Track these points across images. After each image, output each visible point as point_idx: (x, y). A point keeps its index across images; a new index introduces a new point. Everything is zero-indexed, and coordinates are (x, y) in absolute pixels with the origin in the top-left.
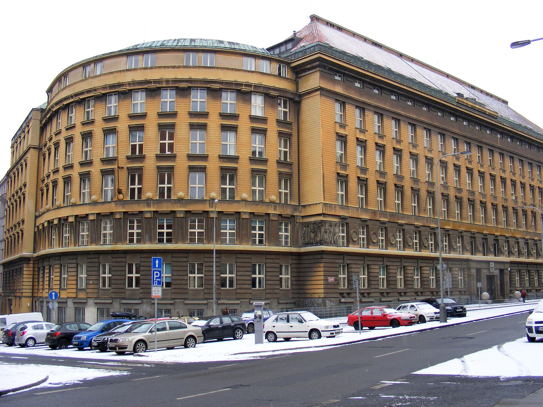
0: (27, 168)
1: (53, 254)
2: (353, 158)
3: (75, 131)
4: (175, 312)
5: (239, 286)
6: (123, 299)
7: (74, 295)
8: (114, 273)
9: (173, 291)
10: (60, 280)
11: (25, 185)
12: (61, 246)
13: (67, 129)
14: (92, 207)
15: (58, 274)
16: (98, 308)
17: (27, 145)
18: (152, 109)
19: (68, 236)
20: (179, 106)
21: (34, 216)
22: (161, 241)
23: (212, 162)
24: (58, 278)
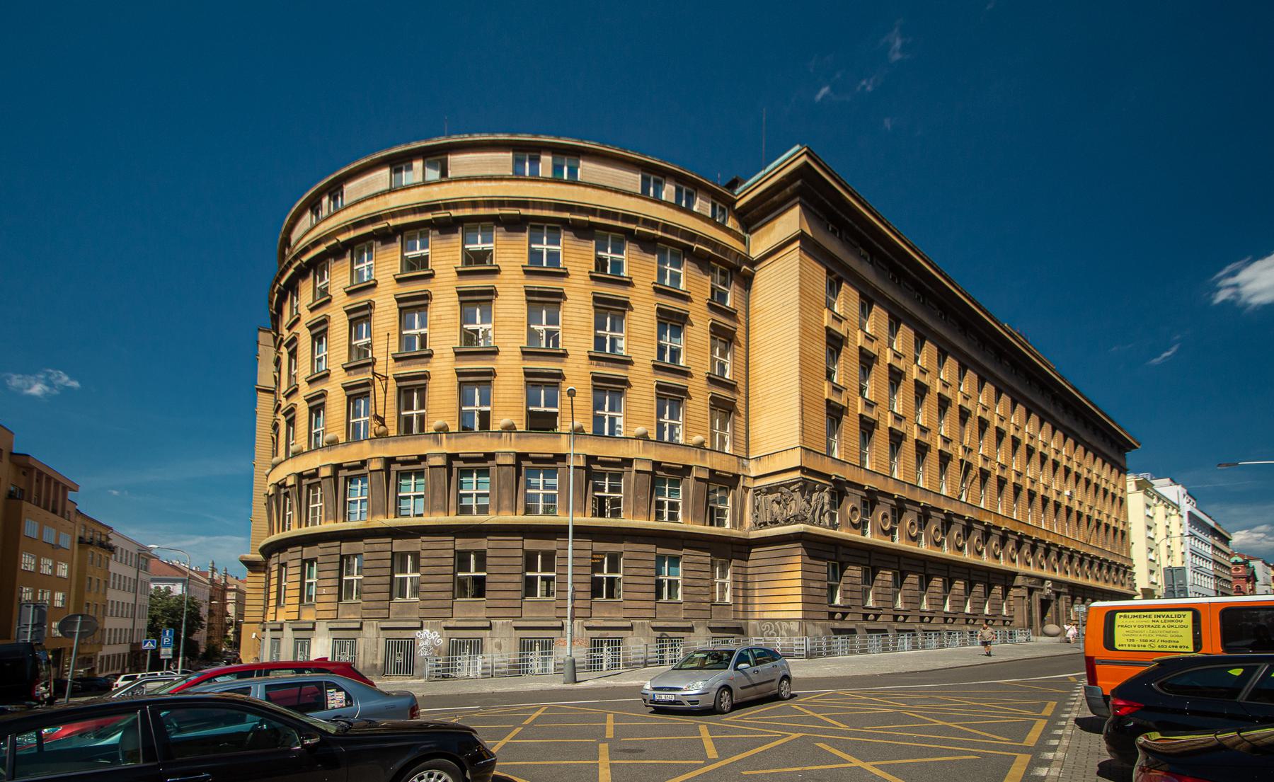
2: (643, 340)
5: (629, 595)
6: (520, 618)
7: (331, 615)
8: (367, 573)
9: (422, 604)
10: (302, 589)
12: (708, 523)
13: (312, 310)
14: (326, 453)
15: (298, 578)
19: (321, 506)
22: (528, 510)
24: (298, 585)
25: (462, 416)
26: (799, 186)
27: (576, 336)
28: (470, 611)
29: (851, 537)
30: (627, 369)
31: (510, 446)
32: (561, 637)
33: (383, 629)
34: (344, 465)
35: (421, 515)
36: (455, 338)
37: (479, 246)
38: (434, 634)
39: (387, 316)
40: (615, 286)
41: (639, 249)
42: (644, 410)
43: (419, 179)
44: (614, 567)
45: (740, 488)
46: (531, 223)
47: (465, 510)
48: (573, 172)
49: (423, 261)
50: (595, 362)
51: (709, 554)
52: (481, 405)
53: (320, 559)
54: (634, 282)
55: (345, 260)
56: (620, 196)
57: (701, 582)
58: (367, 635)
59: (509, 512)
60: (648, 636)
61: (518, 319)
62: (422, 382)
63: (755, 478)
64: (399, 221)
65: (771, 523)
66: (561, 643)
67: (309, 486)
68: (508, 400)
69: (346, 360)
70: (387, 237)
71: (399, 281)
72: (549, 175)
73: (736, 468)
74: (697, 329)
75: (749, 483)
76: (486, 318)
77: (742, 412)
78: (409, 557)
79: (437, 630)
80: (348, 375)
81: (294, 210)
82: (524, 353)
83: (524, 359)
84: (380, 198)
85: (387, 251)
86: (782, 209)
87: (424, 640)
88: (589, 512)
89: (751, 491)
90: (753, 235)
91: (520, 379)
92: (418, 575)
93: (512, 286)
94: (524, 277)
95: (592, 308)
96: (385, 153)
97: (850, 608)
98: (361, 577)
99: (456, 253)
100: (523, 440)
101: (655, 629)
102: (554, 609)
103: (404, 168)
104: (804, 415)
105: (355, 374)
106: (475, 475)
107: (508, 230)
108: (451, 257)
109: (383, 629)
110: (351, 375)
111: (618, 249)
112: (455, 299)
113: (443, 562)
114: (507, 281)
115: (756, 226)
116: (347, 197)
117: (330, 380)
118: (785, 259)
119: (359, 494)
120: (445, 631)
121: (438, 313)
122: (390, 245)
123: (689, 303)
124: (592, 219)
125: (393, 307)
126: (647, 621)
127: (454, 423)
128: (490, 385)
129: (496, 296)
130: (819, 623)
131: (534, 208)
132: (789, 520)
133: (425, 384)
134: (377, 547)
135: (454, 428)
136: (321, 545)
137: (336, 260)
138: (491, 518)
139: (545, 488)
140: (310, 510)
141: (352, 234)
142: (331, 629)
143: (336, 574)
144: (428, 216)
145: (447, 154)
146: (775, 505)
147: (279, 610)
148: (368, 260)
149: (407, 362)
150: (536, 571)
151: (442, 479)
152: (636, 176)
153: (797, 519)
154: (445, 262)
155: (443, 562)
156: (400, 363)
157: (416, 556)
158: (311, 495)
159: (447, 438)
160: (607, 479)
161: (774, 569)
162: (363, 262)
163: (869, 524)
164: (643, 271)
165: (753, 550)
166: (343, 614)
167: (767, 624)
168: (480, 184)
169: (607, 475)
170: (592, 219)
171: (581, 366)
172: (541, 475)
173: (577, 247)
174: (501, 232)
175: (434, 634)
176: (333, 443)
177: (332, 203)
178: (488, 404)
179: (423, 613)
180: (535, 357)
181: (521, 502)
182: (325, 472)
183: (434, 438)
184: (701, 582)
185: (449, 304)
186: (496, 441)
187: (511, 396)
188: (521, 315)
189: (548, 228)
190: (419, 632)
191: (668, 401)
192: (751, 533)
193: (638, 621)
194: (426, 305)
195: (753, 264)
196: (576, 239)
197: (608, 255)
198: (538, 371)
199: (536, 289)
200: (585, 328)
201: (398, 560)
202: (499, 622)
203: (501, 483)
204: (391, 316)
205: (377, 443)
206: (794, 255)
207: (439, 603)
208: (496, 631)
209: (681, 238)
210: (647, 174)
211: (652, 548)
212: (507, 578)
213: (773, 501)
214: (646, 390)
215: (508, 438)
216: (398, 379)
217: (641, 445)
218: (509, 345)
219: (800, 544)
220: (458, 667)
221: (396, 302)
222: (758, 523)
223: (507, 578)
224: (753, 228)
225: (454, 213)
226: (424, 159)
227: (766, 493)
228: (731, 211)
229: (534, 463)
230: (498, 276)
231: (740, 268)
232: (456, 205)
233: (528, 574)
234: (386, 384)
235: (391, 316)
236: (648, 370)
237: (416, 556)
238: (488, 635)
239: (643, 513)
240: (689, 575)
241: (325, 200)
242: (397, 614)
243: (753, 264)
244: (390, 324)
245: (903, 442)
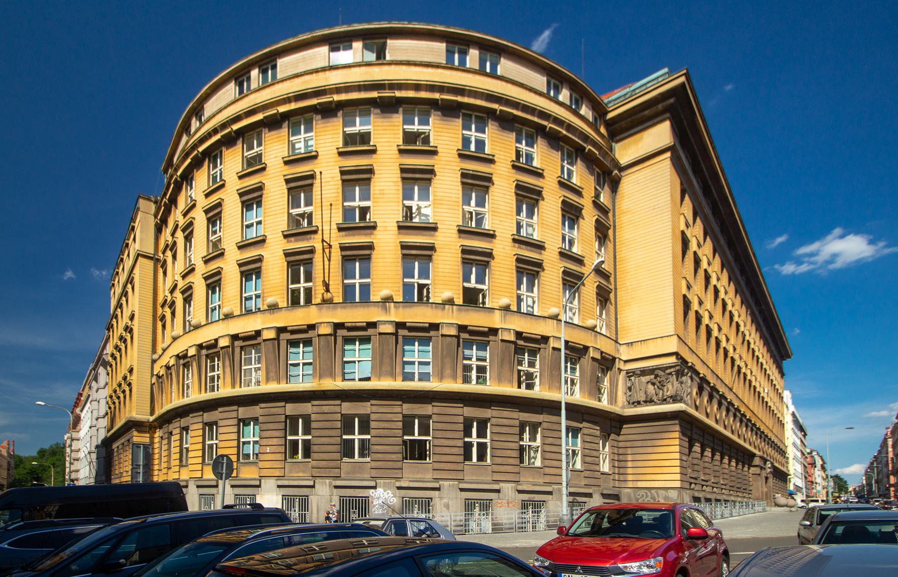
0: (133, 401)
1: (188, 407)
3: (225, 193)
4: (441, 504)
6: (338, 477)
7: (277, 473)
9: (374, 464)
10: (203, 450)
11: (131, 371)
13: (240, 178)
14: (268, 316)
16: (283, 496)
17: (135, 249)
18: (386, 140)
20: (439, 138)
21: (150, 361)
23: (501, 246)
24: (200, 446)
25: (408, 288)
26: (672, 104)
27: (501, 219)
28: (418, 472)
31: (453, 318)
32: (499, 499)
33: (336, 487)
34: (289, 328)
35: (368, 379)
36: (397, 212)
37: (416, 127)
38: (388, 493)
39: (329, 187)
41: (547, 144)
43: (359, 59)
44: (481, 434)
45: (615, 369)
46: (463, 111)
47: (408, 377)
48: (494, 67)
49: (365, 138)
50: (517, 245)
52: (419, 278)
53: (261, 419)
54: (545, 174)
55: (282, 130)
58: (320, 493)
59: (451, 380)
61: (454, 199)
62: (367, 252)
63: (626, 362)
64: (343, 97)
65: (645, 402)
66: (499, 505)
67: (242, 348)
68: (447, 275)
69: (284, 227)
70: (328, 111)
71: (341, 154)
72: (477, 67)
74: (587, 223)
75: (622, 366)
76: (425, 196)
77: (613, 302)
78: (300, 420)
79: (390, 489)
80: (288, 242)
81: (216, 79)
82: (460, 232)
84: (320, 74)
85: (328, 124)
86: (656, 120)
87: (378, 498)
89: (624, 373)
90: (620, 144)
91: (457, 255)
92: (309, 437)
93: (448, 167)
94: (458, 160)
95: (513, 194)
96: (327, 31)
99: (396, 132)
102: (490, 473)
103: (341, 47)
105: (296, 241)
106: (301, 345)
108: (392, 136)
109: (336, 487)
110: (291, 242)
111: (530, 144)
112: (397, 175)
113: (393, 425)
114: (444, 163)
115: (621, 136)
116: (281, 71)
117: (266, 245)
118: (655, 167)
119: (301, 358)
120: (398, 491)
121: (381, 188)
122: (331, 120)
124: (515, 112)
125: (336, 179)
127: (398, 293)
128: (312, 263)
129: (435, 176)
131: (469, 96)
132: (665, 400)
133: (370, 255)
134: (326, 409)
135: (399, 298)
136: (263, 405)
137: (270, 131)
138: (434, 385)
139: (478, 360)
140: (243, 371)
141: (293, 106)
142: (279, 486)
144: (374, 94)
145: (386, 38)
146: (651, 387)
147: (205, 468)
148: (306, 132)
149: (351, 232)
150: (354, 434)
151: (391, 347)
152: (542, 78)
153: (675, 399)
154: (386, 140)
155: (393, 425)
156: (343, 233)
157: (307, 419)
158: (243, 357)
159: (395, 307)
160: (526, 354)
161: (649, 443)
162: (300, 134)
164: (551, 165)
165: (624, 426)
166: (290, 472)
167: (642, 492)
168: (418, 69)
169: (526, 351)
170: (515, 112)
171: (506, 247)
172: (474, 347)
173: (501, 137)
174: (439, 116)
175: (388, 493)
176: (273, 308)
177: (261, 75)
179: (374, 473)
180: (469, 236)
181: (398, 370)
182: (270, 335)
183: (382, 307)
185: (390, 179)
186: (439, 312)
187: (450, 271)
188: (457, 196)
189: (477, 117)
190: (373, 490)
192: (625, 410)
194: (369, 179)
195: (622, 169)
196: (501, 129)
198: (474, 249)
199: (471, 172)
200: (508, 213)
201: (291, 422)
202: (446, 483)
203: (445, 353)
204: (333, 187)
205: (325, 309)
206: (664, 165)
207: (390, 464)
208: (444, 491)
209: (579, 138)
210: (550, 79)
212: (451, 443)
213: (648, 382)
215: (451, 309)
216: (343, 248)
217: (555, 325)
218: (447, 223)
219: (677, 422)
221: (339, 174)
222: (631, 402)
223: (451, 443)
224: (618, 138)
225: (398, 94)
226: (330, 44)
227: (640, 375)
228: (602, 121)
230: (436, 157)
231: (612, 172)
232: (400, 86)
233: (345, 437)
234: (330, 253)
235: (333, 187)
237: (307, 419)
238: (437, 496)
239: (557, 387)
240: (588, 446)
241: (255, 73)
242: (348, 473)
243: (622, 169)
244: (332, 195)
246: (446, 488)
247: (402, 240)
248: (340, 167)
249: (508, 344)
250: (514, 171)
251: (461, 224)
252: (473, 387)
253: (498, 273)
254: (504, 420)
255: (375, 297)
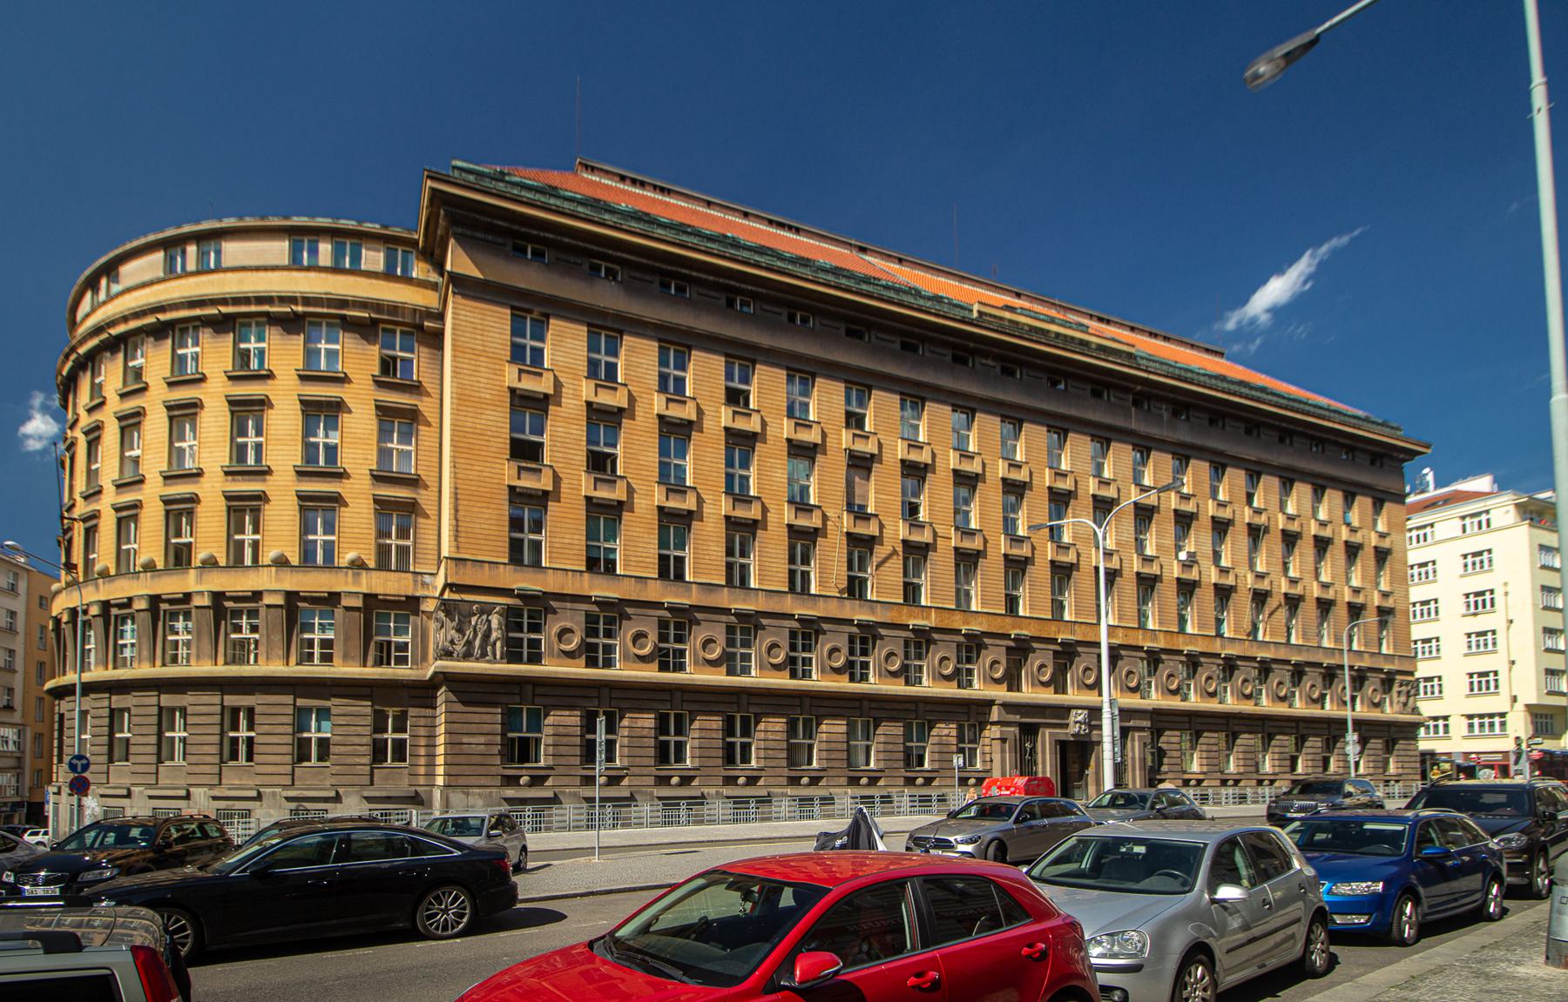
10: (159, 744)
29: (594, 674)
30: (265, 480)
40: (252, 382)
42: (284, 528)
48: (356, 258)
51: (370, 703)
56: (262, 274)
57: (356, 740)
60: (280, 807)
73: (411, 587)
83: (165, 485)
88: (221, 660)
92: (253, 734)
97: (553, 769)
98: (185, 734)
100: (156, 579)
101: (288, 799)
104: (461, 513)
106: (181, 618)
107: (157, 339)
123: (346, 385)
126: (278, 790)
127: (220, 550)
130: (477, 791)
143: (154, 729)
152: (283, 244)
157: (251, 712)
160: (245, 617)
163: (687, 653)
178: (333, 533)
180: (174, 481)
184: (356, 740)
191: (248, 512)
193: (268, 790)
197: (252, 345)
211: (289, 699)
214: (287, 503)
220: (530, 820)
229: (171, 605)
236: (290, 478)
237: (251, 712)
241: (192, 250)
245: (1155, 515)
246: (136, 794)
247: (298, 489)
248: (299, 395)
249: (203, 610)
250: (230, 383)
251: (374, 467)
252: (316, 670)
253: (203, 520)
254: (202, 707)
255: (268, 555)
